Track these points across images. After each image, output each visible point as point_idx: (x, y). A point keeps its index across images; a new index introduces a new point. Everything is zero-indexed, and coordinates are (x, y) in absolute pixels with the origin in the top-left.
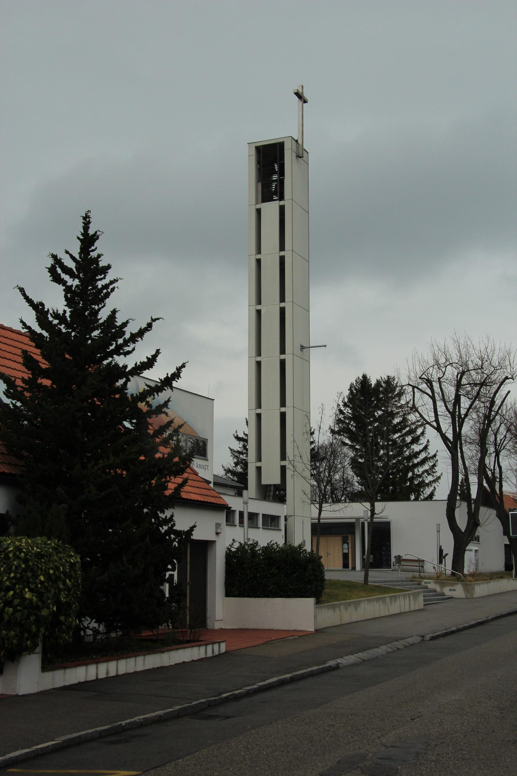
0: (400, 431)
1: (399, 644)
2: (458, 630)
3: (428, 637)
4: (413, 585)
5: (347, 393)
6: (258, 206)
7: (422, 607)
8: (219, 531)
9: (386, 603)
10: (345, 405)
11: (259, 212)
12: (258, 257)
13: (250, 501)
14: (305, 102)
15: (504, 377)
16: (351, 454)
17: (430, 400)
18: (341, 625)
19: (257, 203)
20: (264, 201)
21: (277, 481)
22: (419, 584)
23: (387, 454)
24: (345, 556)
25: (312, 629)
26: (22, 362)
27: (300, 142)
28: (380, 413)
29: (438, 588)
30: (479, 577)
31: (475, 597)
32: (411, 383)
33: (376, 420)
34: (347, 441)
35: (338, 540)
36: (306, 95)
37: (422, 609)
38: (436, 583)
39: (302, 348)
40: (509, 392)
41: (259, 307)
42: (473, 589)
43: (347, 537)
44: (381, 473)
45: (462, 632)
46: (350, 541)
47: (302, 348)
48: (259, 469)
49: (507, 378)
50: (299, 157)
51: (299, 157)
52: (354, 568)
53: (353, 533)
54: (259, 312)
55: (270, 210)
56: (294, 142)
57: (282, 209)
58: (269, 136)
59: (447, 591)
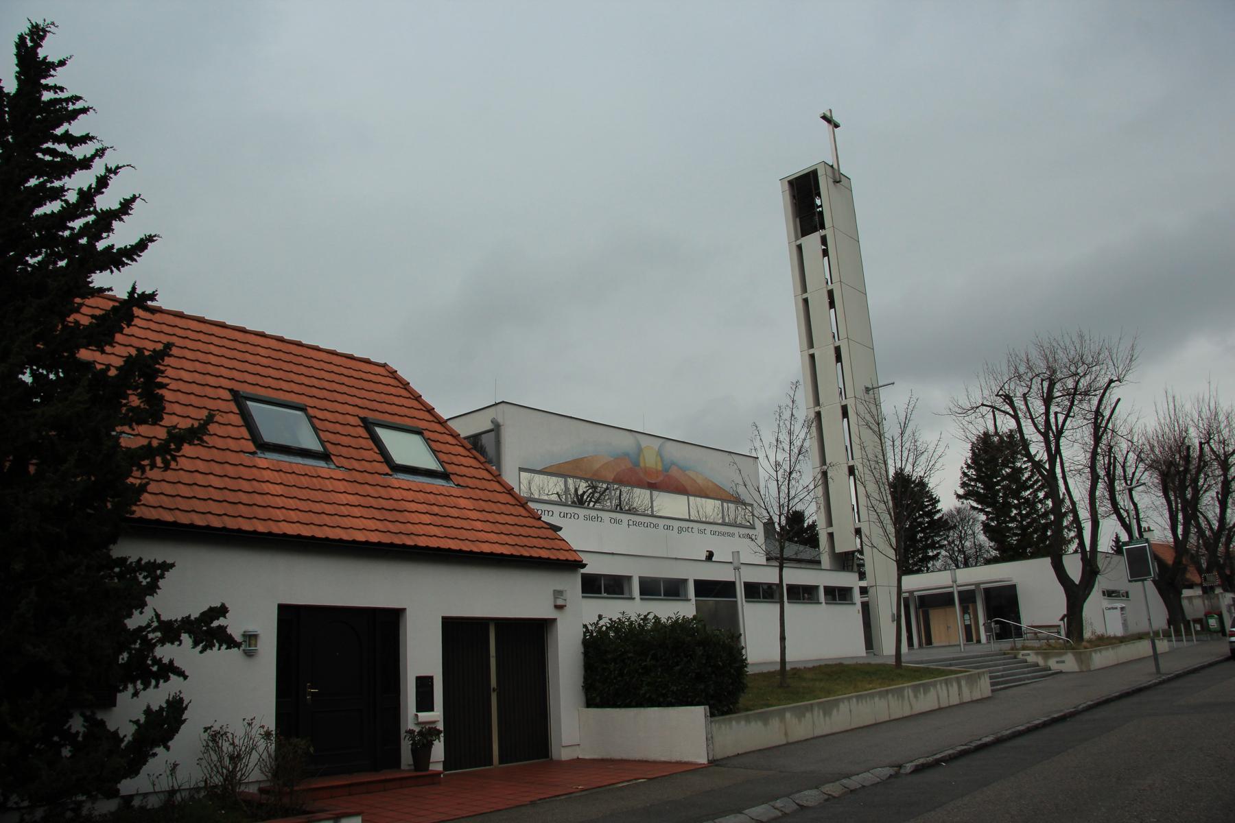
0: (1032, 486)
1: (833, 789)
2: (999, 741)
3: (909, 767)
7: (990, 694)
8: (560, 602)
9: (903, 697)
10: (969, 467)
11: (800, 247)
12: (805, 296)
14: (836, 126)
15: (1107, 380)
16: (983, 517)
17: (1041, 438)
18: (788, 744)
19: (797, 239)
20: (805, 233)
22: (1015, 657)
23: (1020, 514)
24: (968, 629)
25: (704, 761)
27: (835, 166)
28: (1008, 470)
29: (1041, 662)
30: (1103, 641)
31: (1092, 668)
33: (1004, 478)
34: (975, 504)
36: (836, 118)
37: (988, 698)
38: (1037, 654)
39: (867, 390)
40: (1119, 400)
41: (811, 351)
44: (1016, 535)
45: (1008, 744)
46: (971, 611)
47: (867, 390)
48: (831, 535)
49: (1111, 381)
50: (837, 182)
51: (837, 182)
52: (979, 641)
53: (975, 602)
54: (812, 357)
55: (812, 242)
56: (829, 169)
57: (824, 240)
58: (799, 167)
59: (1053, 664)
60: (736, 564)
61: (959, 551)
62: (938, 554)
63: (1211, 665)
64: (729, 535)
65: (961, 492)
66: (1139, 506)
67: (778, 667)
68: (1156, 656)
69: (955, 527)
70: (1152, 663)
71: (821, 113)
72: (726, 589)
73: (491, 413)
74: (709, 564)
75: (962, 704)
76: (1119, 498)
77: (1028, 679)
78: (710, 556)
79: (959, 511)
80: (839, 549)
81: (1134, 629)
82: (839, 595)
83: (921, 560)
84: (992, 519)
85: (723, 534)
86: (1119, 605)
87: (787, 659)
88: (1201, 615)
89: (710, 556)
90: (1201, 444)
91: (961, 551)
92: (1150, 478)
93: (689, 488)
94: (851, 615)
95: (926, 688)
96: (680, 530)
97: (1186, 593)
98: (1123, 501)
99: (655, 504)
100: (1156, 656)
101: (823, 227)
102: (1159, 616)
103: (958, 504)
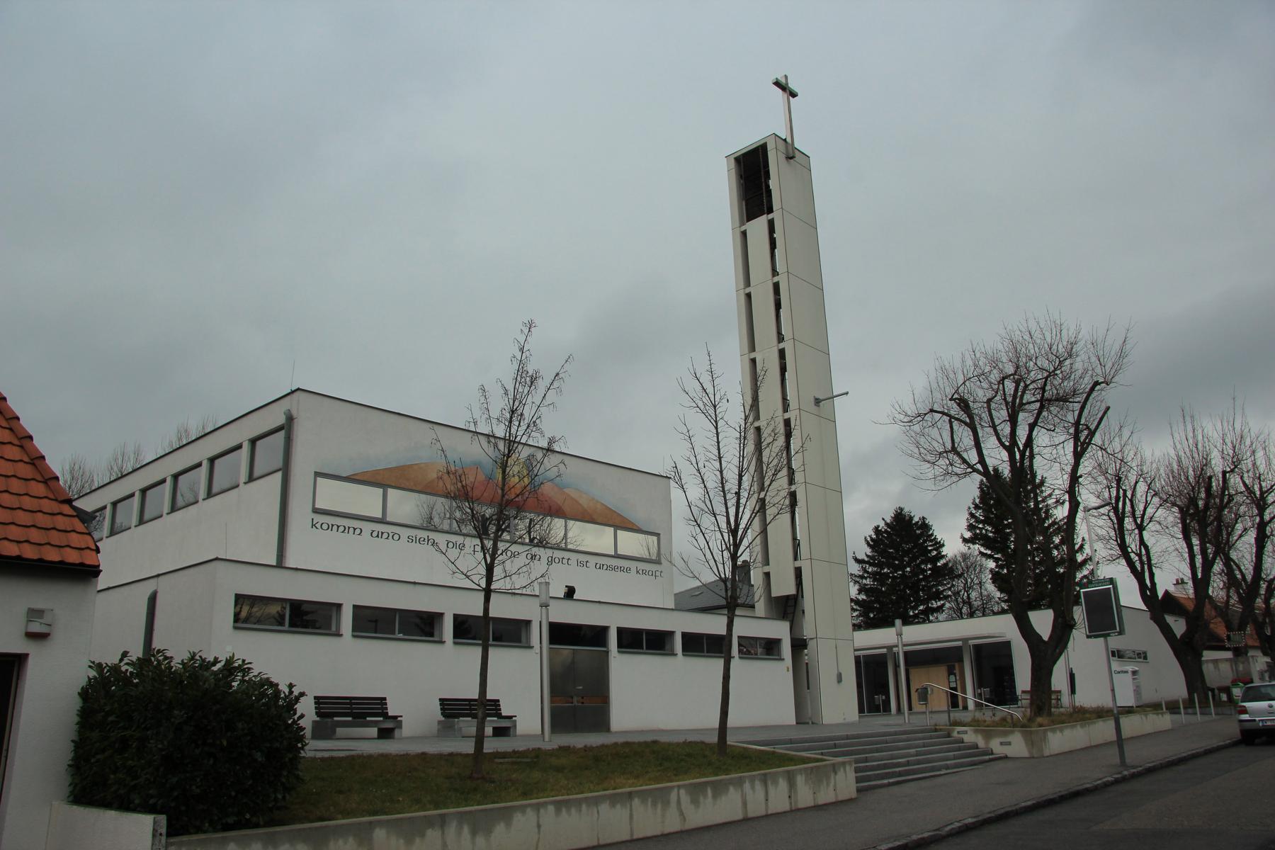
4: (938, 737)
5: (977, 493)
6: (743, 228)
7: (854, 795)
9: (666, 803)
10: (977, 507)
11: (744, 234)
12: (747, 291)
13: (552, 602)
14: (793, 95)
19: (742, 224)
21: (791, 590)
22: (949, 735)
26: (1257, 644)
27: (789, 140)
29: (981, 743)
31: (1047, 753)
32: (936, 408)
34: (982, 549)
35: (941, 671)
36: (792, 85)
37: (851, 800)
38: (976, 731)
39: (817, 402)
40: (1108, 408)
41: (753, 355)
42: (1044, 739)
43: (954, 667)
46: (957, 671)
47: (817, 402)
50: (790, 158)
52: (965, 708)
53: (961, 660)
55: (758, 227)
57: (771, 224)
59: (996, 746)
60: (543, 598)
61: (964, 602)
62: (943, 605)
63: (1208, 752)
64: (622, 569)
65: (968, 535)
66: (1152, 552)
67: (714, 739)
68: (1120, 741)
69: (960, 576)
70: (1115, 750)
71: (773, 79)
72: (597, 635)
73: (285, 405)
74: (569, 603)
75: (795, 811)
76: (1128, 540)
77: (947, 767)
78: (570, 593)
79: (965, 557)
80: (776, 592)
81: (1149, 696)
82: (771, 648)
83: (922, 612)
84: (1001, 567)
85: (614, 569)
86: (1130, 668)
87: (732, 721)
88: (1227, 683)
89: (570, 593)
90: (1224, 473)
91: (968, 602)
92: (1169, 516)
93: (566, 508)
94: (779, 673)
95: (719, 789)
96: (330, 527)
97: (1208, 655)
98: (1132, 543)
99: (570, 535)
100: (1120, 741)
101: (770, 210)
102: (1173, 684)
103: (963, 548)
